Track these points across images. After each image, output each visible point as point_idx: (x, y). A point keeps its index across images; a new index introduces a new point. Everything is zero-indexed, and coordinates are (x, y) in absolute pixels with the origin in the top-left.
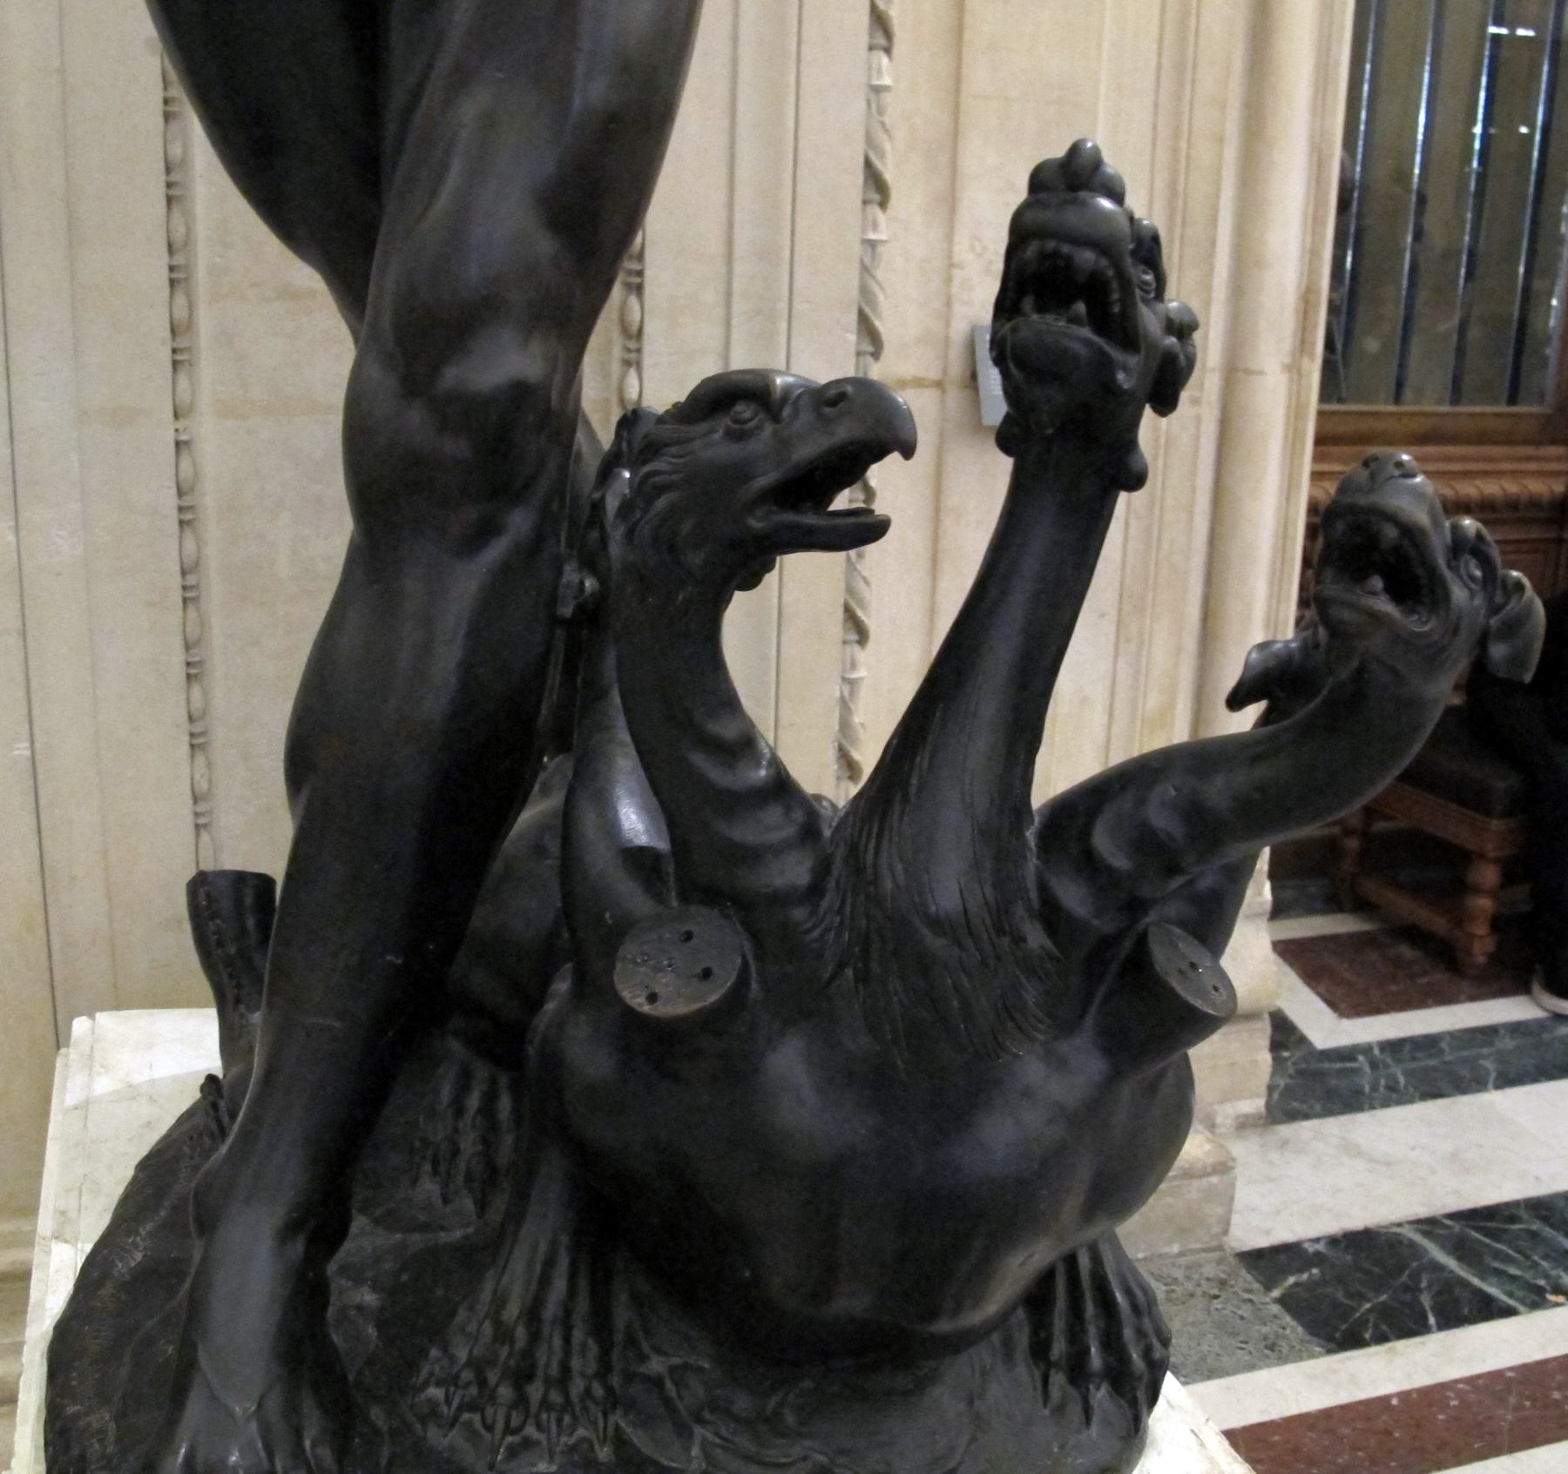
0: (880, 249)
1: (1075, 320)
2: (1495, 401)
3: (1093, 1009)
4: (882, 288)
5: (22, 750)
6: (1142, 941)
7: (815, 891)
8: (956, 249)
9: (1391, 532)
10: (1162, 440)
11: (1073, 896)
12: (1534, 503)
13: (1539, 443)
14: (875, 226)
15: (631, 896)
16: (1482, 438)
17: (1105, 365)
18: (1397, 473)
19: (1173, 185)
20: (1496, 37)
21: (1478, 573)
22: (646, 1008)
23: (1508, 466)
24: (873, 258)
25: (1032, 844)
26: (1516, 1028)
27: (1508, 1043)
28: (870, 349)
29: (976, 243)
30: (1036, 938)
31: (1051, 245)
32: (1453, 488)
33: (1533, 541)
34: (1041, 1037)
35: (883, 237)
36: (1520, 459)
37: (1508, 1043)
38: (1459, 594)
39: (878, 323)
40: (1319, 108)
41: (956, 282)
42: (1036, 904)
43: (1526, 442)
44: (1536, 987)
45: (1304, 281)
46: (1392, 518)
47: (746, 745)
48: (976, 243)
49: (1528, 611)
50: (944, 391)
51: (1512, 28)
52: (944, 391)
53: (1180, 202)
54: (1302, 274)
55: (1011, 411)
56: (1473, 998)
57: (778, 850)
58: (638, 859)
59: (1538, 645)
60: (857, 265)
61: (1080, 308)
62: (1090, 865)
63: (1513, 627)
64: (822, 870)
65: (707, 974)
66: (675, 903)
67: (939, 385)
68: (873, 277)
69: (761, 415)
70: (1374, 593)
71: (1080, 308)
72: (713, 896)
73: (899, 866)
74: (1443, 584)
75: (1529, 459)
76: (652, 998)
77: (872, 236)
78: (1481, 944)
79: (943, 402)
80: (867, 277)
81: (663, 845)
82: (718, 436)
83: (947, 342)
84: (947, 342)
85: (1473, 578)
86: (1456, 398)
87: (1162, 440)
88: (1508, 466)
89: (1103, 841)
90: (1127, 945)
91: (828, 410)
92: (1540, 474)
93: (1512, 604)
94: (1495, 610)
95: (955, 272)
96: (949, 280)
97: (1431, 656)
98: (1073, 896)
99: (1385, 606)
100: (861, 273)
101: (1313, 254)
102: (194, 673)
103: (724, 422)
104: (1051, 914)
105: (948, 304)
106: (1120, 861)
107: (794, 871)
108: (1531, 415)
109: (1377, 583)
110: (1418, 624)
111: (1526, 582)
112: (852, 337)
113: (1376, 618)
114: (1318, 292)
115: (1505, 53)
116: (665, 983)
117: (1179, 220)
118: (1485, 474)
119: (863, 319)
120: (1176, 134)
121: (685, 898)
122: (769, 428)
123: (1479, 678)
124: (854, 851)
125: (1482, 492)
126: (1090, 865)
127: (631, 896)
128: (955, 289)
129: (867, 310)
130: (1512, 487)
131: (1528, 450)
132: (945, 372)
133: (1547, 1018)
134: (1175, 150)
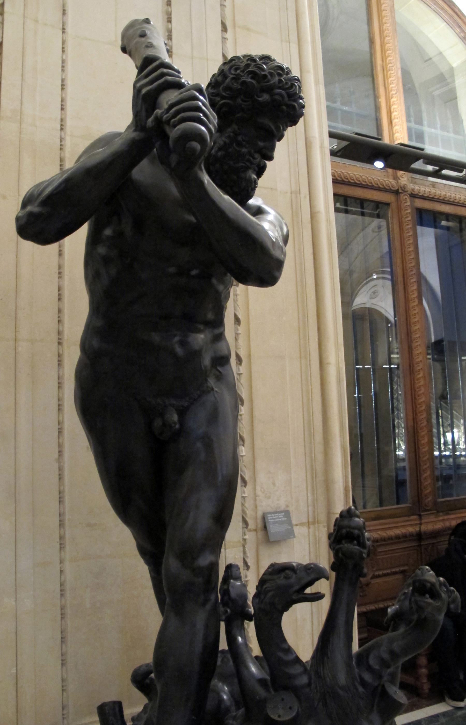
0: (246, 498)
1: (354, 545)
2: (393, 505)
3: (375, 706)
4: (247, 509)
5: (14, 671)
6: (383, 686)
7: (309, 684)
8: (257, 491)
9: (429, 585)
10: (317, 539)
11: (367, 677)
12: (411, 535)
13: (409, 516)
14: (244, 492)
15: (261, 692)
16: (391, 516)
17: (361, 553)
18: (427, 571)
19: (312, 466)
20: (358, 369)
21: (445, 590)
22: (279, 719)
23: (403, 524)
24: (244, 501)
25: (355, 665)
26: (444, 714)
27: (443, 720)
28: (245, 526)
29: (262, 489)
30: (361, 689)
31: (348, 530)
32: (386, 533)
33: (414, 546)
34: (365, 715)
35: (247, 495)
36: (405, 521)
37: (443, 720)
38: (443, 595)
39: (247, 519)
40: (342, 436)
41: (258, 500)
42: (359, 680)
43: (406, 516)
44: (447, 699)
45: (344, 484)
46: (426, 581)
47: (289, 650)
48: (262, 489)
49: (456, 597)
50: (257, 533)
51: (364, 365)
52: (257, 533)
53: (314, 472)
54: (344, 482)
55: (335, 561)
56: (428, 705)
57: (300, 675)
58: (262, 682)
59: (460, 604)
60: (241, 504)
61: (355, 542)
62: (370, 669)
63: (454, 601)
64: (310, 678)
65: (290, 708)
66: (273, 692)
67: (255, 530)
68: (244, 506)
69: (292, 573)
70: (427, 598)
71: (355, 542)
72: (286, 688)
73: (330, 675)
74: (440, 594)
75: (408, 521)
76: (279, 716)
77: (244, 495)
78: (426, 687)
79: (257, 535)
80: (243, 507)
81: (268, 678)
82: (282, 578)
83: (256, 518)
84: (256, 518)
85: (445, 591)
86: (381, 504)
87: (317, 539)
88: (403, 524)
89: (372, 661)
90: (380, 688)
91: (308, 571)
92: (411, 525)
93: (453, 595)
94: (449, 597)
95: (257, 498)
96: (255, 500)
97: (439, 610)
98: (367, 677)
99: (430, 601)
100: (242, 506)
101: (346, 477)
102: (63, 640)
103: (283, 575)
104: (363, 683)
105: (256, 507)
106: (377, 667)
107: (304, 680)
108: (404, 507)
109: (427, 596)
110: (437, 604)
111: (455, 590)
112: (241, 524)
113: (430, 604)
114: (349, 487)
115: (361, 373)
116: (281, 712)
117: (314, 476)
118: (395, 527)
119: (243, 518)
120: (311, 453)
121: (276, 690)
122: (294, 576)
123: (449, 614)
124: (317, 672)
125: (395, 533)
126: (370, 669)
127: (261, 692)
128: (258, 503)
129: (244, 515)
130: (404, 531)
131: (406, 518)
132: (257, 526)
133: (453, 709)
134: (311, 457)
